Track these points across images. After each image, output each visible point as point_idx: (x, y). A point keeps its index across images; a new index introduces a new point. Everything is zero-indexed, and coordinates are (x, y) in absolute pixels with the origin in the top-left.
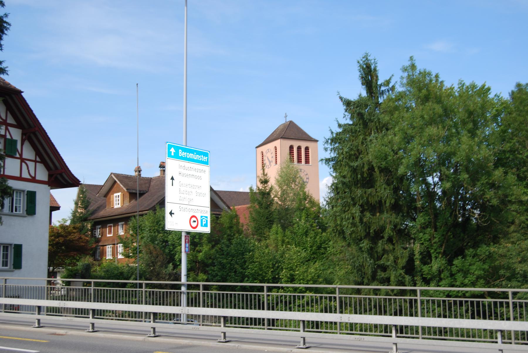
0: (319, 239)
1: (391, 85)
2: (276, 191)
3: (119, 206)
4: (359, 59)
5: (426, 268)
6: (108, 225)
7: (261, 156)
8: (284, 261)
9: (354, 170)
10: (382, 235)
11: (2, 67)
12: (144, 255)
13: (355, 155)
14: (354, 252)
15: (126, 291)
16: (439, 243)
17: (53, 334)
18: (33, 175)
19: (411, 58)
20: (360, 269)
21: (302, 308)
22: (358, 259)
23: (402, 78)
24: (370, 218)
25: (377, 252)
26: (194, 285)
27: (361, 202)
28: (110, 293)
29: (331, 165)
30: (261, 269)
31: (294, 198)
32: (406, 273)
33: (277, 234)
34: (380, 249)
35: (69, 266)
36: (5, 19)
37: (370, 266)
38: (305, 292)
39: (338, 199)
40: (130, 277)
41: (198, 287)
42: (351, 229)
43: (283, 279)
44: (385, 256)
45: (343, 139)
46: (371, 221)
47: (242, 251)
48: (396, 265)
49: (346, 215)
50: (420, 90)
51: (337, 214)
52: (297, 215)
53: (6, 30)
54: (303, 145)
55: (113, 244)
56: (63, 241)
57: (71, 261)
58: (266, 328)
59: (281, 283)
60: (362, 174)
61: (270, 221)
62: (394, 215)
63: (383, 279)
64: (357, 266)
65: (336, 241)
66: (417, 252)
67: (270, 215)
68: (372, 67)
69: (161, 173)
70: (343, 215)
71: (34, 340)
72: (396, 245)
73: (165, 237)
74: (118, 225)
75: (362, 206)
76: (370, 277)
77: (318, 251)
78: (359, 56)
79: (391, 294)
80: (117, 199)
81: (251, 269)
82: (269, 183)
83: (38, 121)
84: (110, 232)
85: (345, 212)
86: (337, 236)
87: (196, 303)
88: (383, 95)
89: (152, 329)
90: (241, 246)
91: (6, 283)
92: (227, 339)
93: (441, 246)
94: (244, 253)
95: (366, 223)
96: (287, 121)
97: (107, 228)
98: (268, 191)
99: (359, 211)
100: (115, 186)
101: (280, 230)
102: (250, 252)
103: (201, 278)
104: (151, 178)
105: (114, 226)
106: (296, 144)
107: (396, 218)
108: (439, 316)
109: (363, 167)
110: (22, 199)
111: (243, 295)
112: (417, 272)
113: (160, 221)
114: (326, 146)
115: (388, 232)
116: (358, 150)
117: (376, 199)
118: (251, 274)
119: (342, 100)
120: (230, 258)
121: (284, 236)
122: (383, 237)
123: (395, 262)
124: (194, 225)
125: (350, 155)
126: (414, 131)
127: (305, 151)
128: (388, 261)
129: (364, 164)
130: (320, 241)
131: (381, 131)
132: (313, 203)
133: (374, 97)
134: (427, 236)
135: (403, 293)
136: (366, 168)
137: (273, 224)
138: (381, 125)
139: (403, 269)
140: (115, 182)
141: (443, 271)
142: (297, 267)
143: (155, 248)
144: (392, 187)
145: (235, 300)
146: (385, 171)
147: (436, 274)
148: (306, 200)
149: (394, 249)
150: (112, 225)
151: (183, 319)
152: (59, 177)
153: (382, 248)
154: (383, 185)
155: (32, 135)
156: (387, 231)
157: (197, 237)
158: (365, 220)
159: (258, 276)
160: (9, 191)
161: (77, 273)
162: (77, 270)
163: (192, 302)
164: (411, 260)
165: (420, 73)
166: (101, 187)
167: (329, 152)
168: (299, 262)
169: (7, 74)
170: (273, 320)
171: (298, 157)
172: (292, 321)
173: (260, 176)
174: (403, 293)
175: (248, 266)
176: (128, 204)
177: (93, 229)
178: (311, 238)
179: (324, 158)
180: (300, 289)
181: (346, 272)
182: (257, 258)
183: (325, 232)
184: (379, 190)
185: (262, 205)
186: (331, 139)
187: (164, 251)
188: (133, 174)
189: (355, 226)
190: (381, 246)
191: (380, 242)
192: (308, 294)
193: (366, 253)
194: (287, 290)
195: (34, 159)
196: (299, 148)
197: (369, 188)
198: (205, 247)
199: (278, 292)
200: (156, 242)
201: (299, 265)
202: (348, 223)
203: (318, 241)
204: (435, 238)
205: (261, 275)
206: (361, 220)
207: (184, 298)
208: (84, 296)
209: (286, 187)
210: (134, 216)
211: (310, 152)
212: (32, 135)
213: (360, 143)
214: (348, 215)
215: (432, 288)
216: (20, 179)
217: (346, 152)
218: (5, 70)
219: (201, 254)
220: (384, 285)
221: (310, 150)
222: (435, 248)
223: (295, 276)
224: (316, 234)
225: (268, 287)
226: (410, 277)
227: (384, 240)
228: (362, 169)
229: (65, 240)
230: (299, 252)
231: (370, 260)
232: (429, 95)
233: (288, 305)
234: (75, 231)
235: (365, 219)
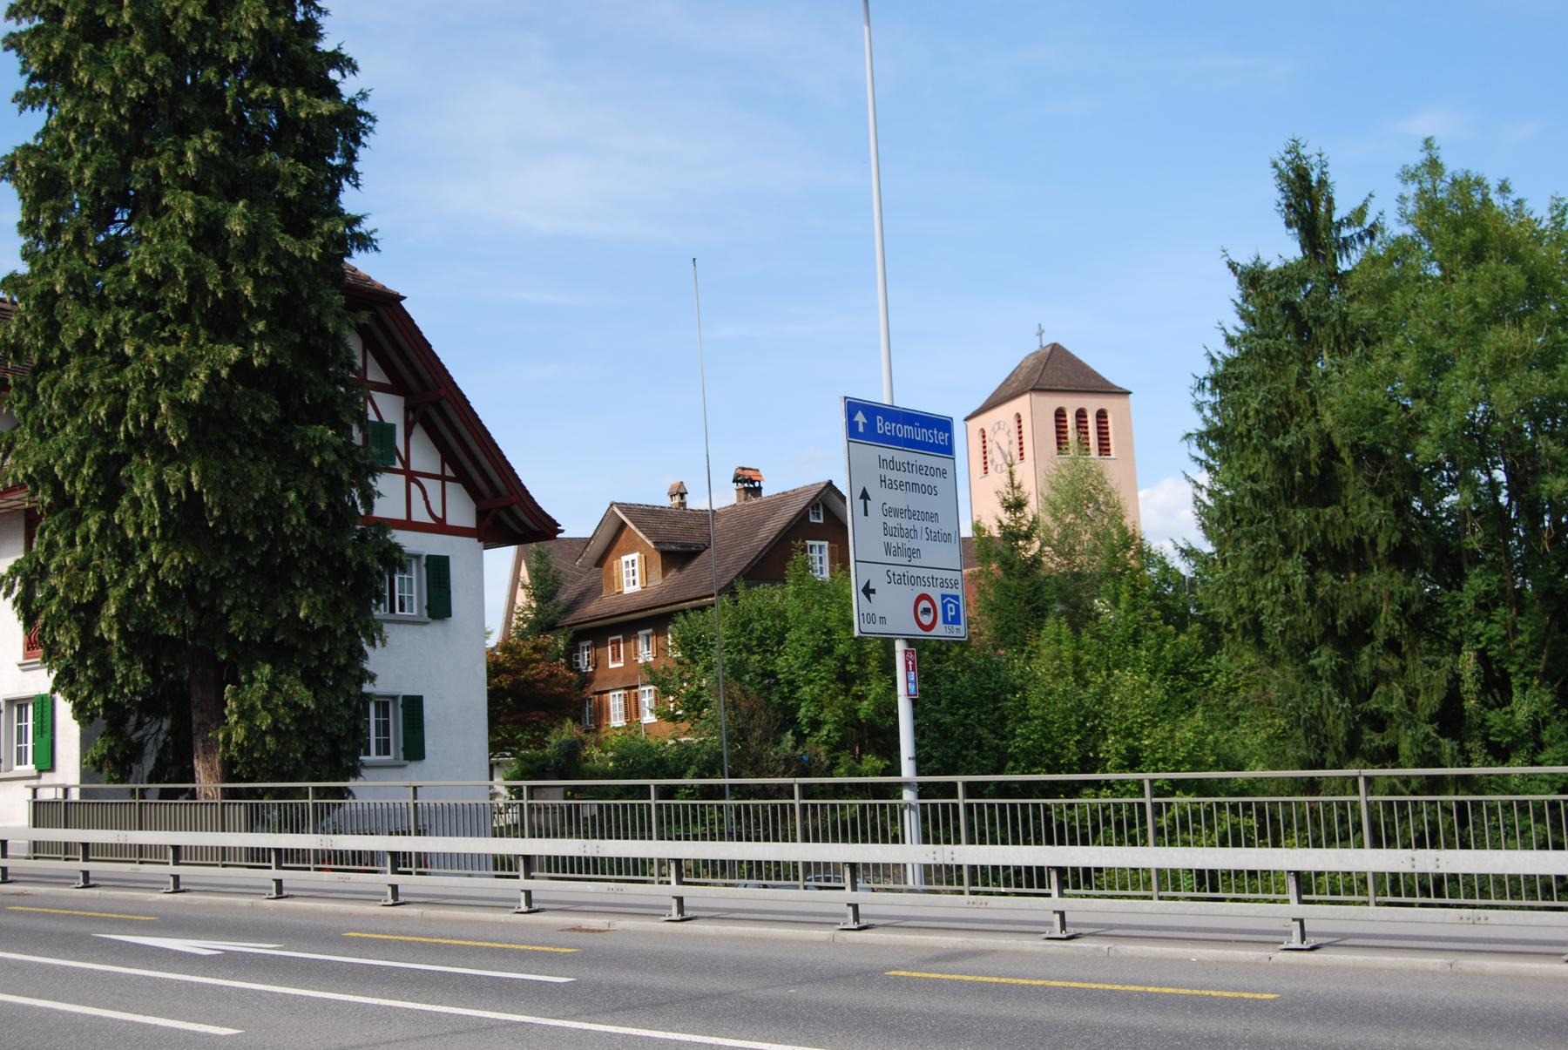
0: (1171, 649)
1: (1368, 221)
2: (1048, 530)
3: (637, 588)
4: (1276, 157)
5: (1495, 718)
6: (610, 639)
7: (981, 440)
8: (1107, 712)
9: (1284, 460)
10: (1368, 631)
11: (363, 231)
12: (716, 709)
13: (1281, 416)
14: (1291, 680)
15: (677, 806)
16: (1532, 647)
17: (574, 930)
18: (440, 515)
19: (1428, 143)
20: (1313, 727)
21: (1166, 837)
22: (1305, 700)
23: (1402, 199)
24: (1333, 586)
25: (1356, 678)
26: (850, 784)
27: (1307, 543)
28: (633, 814)
30: (1047, 737)
31: (1096, 545)
32: (1441, 732)
33: (1059, 642)
34: (1364, 671)
35: (527, 747)
36: (360, 106)
37: (1343, 717)
38: (1173, 794)
39: (1238, 540)
40: (685, 771)
41: (950, 790)
42: (1284, 620)
43: (1108, 760)
44: (1382, 688)
45: (1246, 377)
46: (1338, 595)
48: (1414, 711)
50: (1457, 228)
51: (1240, 580)
52: (1107, 589)
53: (365, 134)
54: (1092, 404)
55: (626, 688)
56: (511, 685)
57: (533, 736)
58: (967, 892)
59: (1104, 771)
60: (1305, 468)
62: (1399, 577)
63: (1380, 752)
64: (1305, 720)
65: (1237, 654)
66: (1469, 674)
68: (1314, 177)
69: (739, 496)
70: (1259, 584)
71: (444, 941)
72: (1409, 658)
73: (768, 663)
74: (637, 638)
75: (1310, 555)
76: (1341, 748)
78: (1277, 149)
79: (1404, 790)
81: (1023, 737)
82: (1026, 509)
83: (446, 371)
84: (616, 657)
85: (1263, 572)
86: (1240, 639)
87: (642, 830)
88: (1347, 249)
89: (675, 902)
90: (990, 677)
91: (415, 797)
92: (864, 922)
93: (1536, 654)
94: (999, 694)
95: (1323, 600)
96: (1044, 345)
98: (1025, 528)
99: (1304, 568)
100: (623, 536)
101: (1066, 630)
102: (1014, 694)
103: (868, 767)
105: (625, 641)
106: (1071, 404)
107: (1408, 584)
108: (1543, 846)
109: (1307, 448)
110: (414, 577)
111: (1002, 806)
112: (1470, 729)
113: (750, 621)
114: (1199, 396)
115: (1386, 621)
116: (1288, 404)
117: (1351, 534)
119: (1234, 270)
120: (962, 711)
121: (1079, 648)
122: (1370, 638)
123: (1409, 702)
124: (926, 620)
125: (1269, 419)
126: (1452, 341)
127: (1098, 422)
128: (1391, 700)
129: (1308, 440)
130: (1174, 656)
131: (1352, 349)
132: (1145, 555)
133: (1324, 257)
134: (1496, 630)
135: (1435, 785)
136: (1314, 453)
137: (1044, 616)
138: (1349, 332)
139: (1431, 722)
140: (623, 525)
141: (1546, 722)
143: (743, 691)
144: (1391, 498)
145: (982, 823)
146: (1370, 456)
147: (1526, 731)
148: (1128, 548)
149: (1403, 669)
150: (620, 637)
151: (913, 879)
152: (504, 515)
153: (1371, 666)
154: (1364, 494)
155: (432, 412)
156: (1382, 621)
157: (852, 659)
158: (1320, 592)
159: (1041, 755)
160: (397, 555)
161: (545, 766)
162: (544, 757)
163: (937, 828)
164: (1453, 697)
165: (1455, 181)
166: (586, 542)
169: (376, 249)
170: (1087, 870)
171: (1099, 439)
172: (1340, 877)
173: (1004, 490)
174: (1435, 785)
178: (1148, 650)
181: (1269, 738)
182: (1036, 708)
183: (1185, 632)
184: (1353, 508)
185: (1012, 567)
187: (768, 700)
188: (666, 502)
189: (1292, 612)
191: (1367, 649)
192: (1180, 799)
193: (1327, 681)
194: (1122, 790)
195: (438, 472)
196: (1081, 415)
197: (1325, 506)
198: (874, 683)
199: (1097, 796)
200: (747, 678)
202: (1274, 603)
204: (1521, 632)
205: (1051, 751)
206: (1310, 595)
207: (911, 822)
208: (571, 825)
209: (1071, 516)
210: (684, 612)
211: (1110, 424)
212: (432, 412)
213: (1293, 385)
215: (1515, 770)
216: (409, 525)
217: (1257, 412)
218: (371, 240)
219: (865, 703)
220: (1385, 767)
221: (1110, 419)
222: (1522, 659)
223: (1141, 751)
224: (1163, 639)
225: (967, 785)
226: (1455, 744)
227: (1376, 644)
229: (515, 680)
231: (1342, 701)
232: (1484, 239)
233: (1127, 830)
234: (537, 656)
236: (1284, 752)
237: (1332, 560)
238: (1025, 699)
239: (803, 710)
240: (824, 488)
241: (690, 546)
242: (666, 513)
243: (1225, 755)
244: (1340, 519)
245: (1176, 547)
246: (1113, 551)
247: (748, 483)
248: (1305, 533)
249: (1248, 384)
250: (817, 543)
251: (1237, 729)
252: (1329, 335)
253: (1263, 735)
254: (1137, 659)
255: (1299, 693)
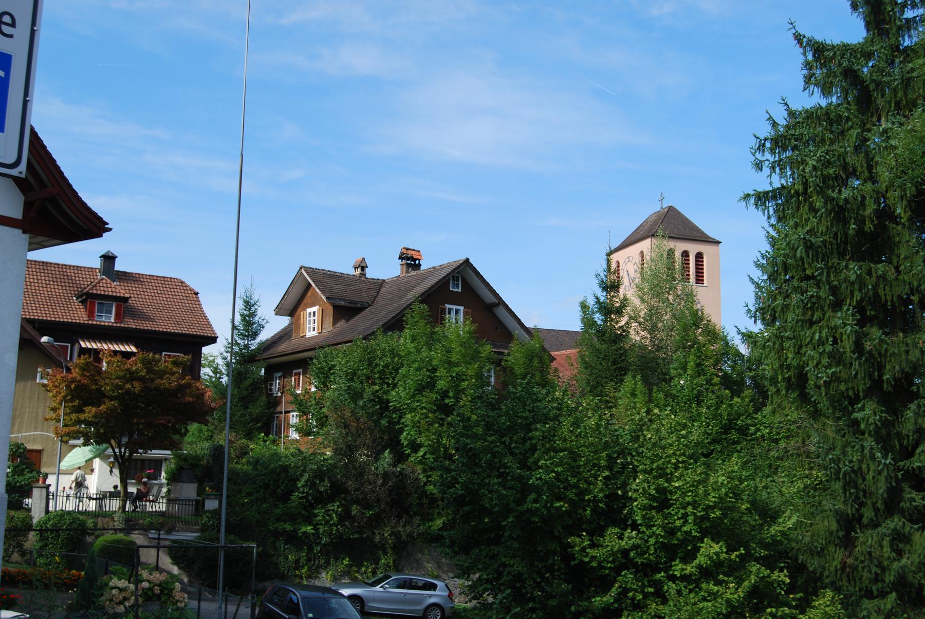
2: (635, 310)
3: (315, 333)
6: (295, 371)
9: (840, 213)
14: (830, 433)
24: (882, 341)
27: (857, 296)
29: (771, 209)
37: (885, 473)
42: (830, 372)
43: (636, 500)
46: (886, 350)
47: (526, 418)
49: (814, 333)
51: (787, 334)
54: (693, 249)
60: (861, 222)
61: (621, 369)
63: (919, 511)
64: (845, 474)
65: (779, 406)
67: (621, 357)
69: (402, 270)
76: (880, 505)
77: (724, 436)
80: (312, 318)
85: (811, 323)
86: (784, 392)
88: (909, 30)
94: (531, 424)
95: (870, 352)
96: (664, 207)
97: (291, 377)
98: (617, 305)
104: (384, 281)
106: (679, 247)
109: (863, 204)
114: (759, 156)
116: (845, 166)
118: (546, 482)
119: (800, 42)
125: (825, 178)
129: (863, 197)
130: (729, 414)
132: (713, 334)
137: (625, 374)
140: (309, 285)
142: (676, 468)
148: (698, 327)
150: (301, 370)
153: (916, 423)
154: (917, 252)
157: (451, 394)
158: (868, 346)
167: (766, 170)
168: (684, 454)
173: (603, 274)
175: (539, 460)
176: (329, 329)
177: (269, 377)
178: (708, 408)
179: (752, 193)
180: (686, 532)
181: (805, 487)
186: (772, 139)
187: (378, 423)
190: (912, 421)
191: (913, 406)
193: (870, 435)
196: (685, 254)
201: (683, 462)
202: (821, 354)
203: (725, 414)
205: (575, 486)
206: (858, 347)
214: (820, 332)
221: (705, 259)
223: (671, 493)
228: (858, 209)
230: (685, 426)
231: (885, 456)
235: (868, 343)
236: (820, 503)
237: (882, 316)
238: (554, 429)
239: (405, 434)
240: (462, 264)
241: (356, 303)
242: (344, 278)
243: (762, 501)
244: (891, 274)
245: (739, 332)
246: (686, 328)
247: (410, 260)
248: (856, 286)
249: (807, 144)
250: (455, 307)
251: (776, 478)
252: (890, 103)
253: (800, 485)
254: (699, 415)
255: (839, 446)
